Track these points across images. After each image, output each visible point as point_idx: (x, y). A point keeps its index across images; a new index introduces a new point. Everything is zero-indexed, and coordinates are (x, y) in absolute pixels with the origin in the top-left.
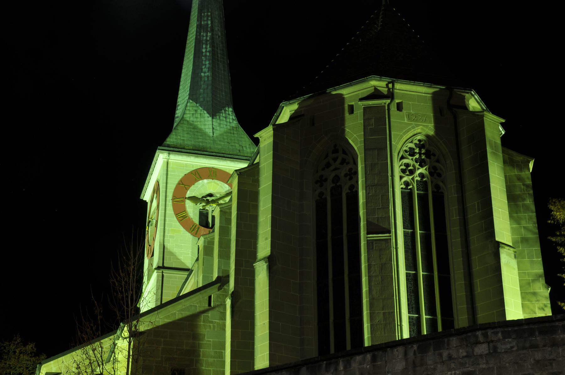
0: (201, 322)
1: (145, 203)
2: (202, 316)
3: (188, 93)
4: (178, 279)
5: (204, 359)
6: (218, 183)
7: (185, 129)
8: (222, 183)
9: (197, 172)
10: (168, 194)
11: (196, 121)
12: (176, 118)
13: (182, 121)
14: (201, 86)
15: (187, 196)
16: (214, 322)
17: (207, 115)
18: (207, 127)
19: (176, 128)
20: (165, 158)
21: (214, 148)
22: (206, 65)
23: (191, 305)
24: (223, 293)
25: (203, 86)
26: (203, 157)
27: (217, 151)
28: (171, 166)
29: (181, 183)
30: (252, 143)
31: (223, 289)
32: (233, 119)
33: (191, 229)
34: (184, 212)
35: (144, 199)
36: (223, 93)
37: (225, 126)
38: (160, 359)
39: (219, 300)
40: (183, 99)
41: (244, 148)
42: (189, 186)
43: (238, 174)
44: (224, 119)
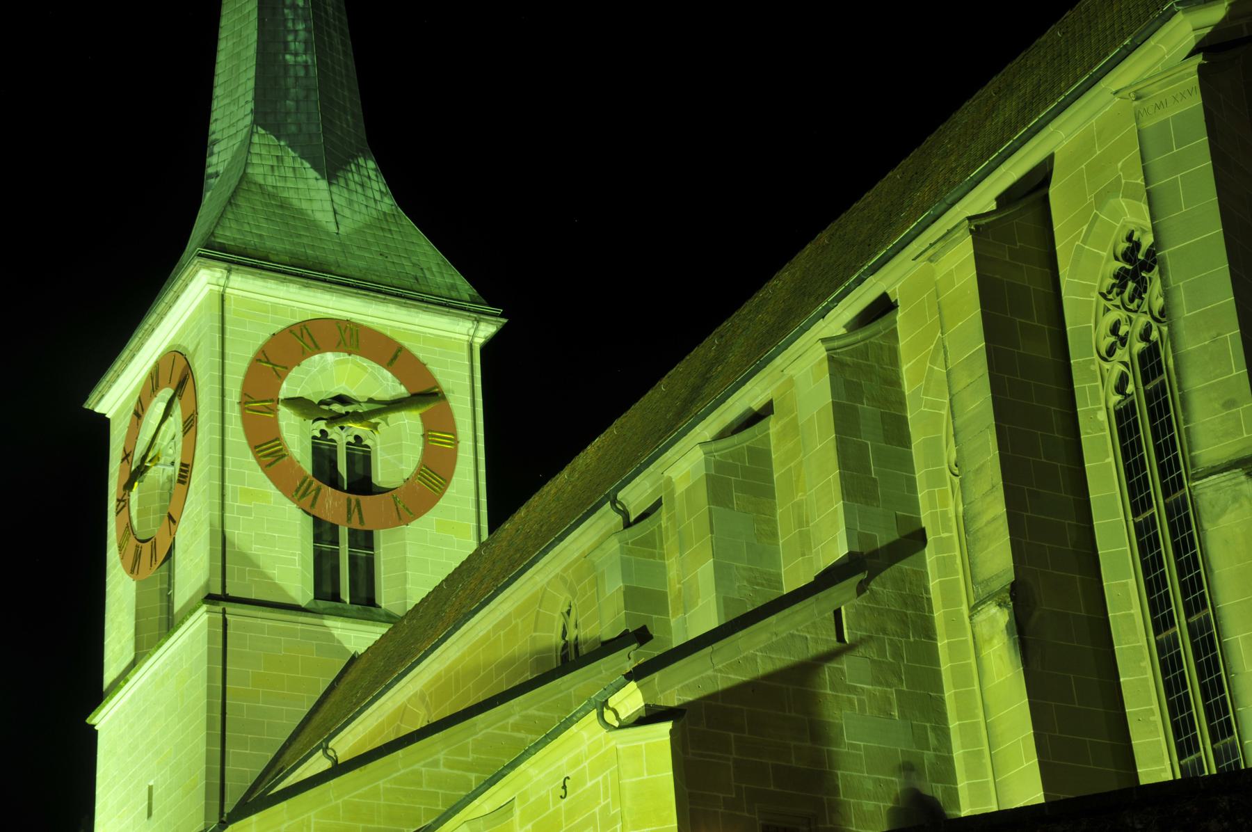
0: (826, 689)
1: (102, 423)
2: (826, 670)
3: (251, 106)
4: (268, 634)
5: (852, 800)
6: (365, 364)
7: (259, 207)
8: (376, 366)
9: (306, 329)
10: (227, 387)
11: (283, 187)
12: (211, 176)
13: (244, 183)
14: (287, 89)
15: (281, 397)
16: (860, 690)
17: (312, 173)
18: (317, 206)
19: (232, 201)
20: (215, 282)
21: (349, 266)
22: (296, 32)
23: (792, 636)
24: (870, 605)
25: (293, 91)
26: (324, 289)
27: (357, 275)
28: (233, 307)
29: (263, 359)
30: (443, 261)
31: (868, 591)
32: (381, 192)
33: (297, 491)
34: (278, 442)
35: (97, 410)
36: (349, 117)
37: (364, 210)
38: (734, 796)
39: (863, 624)
40: (233, 125)
41: (426, 271)
42: (286, 368)
43: (971, 231)
44: (359, 189)
